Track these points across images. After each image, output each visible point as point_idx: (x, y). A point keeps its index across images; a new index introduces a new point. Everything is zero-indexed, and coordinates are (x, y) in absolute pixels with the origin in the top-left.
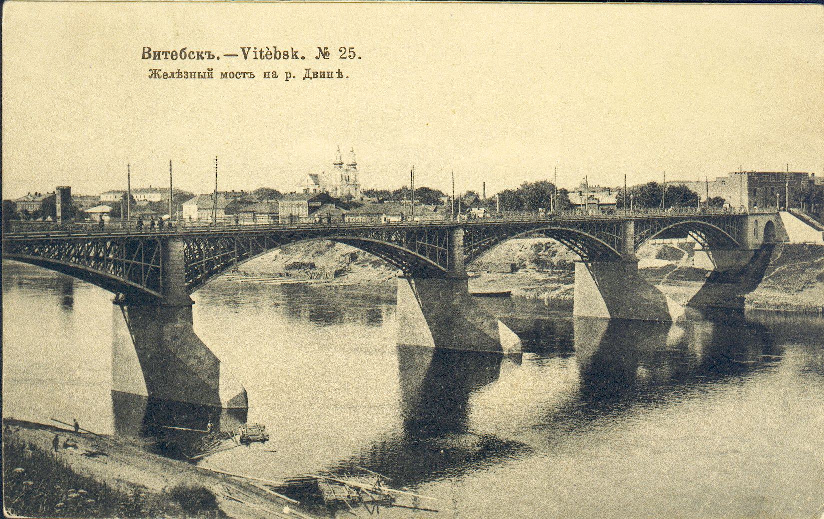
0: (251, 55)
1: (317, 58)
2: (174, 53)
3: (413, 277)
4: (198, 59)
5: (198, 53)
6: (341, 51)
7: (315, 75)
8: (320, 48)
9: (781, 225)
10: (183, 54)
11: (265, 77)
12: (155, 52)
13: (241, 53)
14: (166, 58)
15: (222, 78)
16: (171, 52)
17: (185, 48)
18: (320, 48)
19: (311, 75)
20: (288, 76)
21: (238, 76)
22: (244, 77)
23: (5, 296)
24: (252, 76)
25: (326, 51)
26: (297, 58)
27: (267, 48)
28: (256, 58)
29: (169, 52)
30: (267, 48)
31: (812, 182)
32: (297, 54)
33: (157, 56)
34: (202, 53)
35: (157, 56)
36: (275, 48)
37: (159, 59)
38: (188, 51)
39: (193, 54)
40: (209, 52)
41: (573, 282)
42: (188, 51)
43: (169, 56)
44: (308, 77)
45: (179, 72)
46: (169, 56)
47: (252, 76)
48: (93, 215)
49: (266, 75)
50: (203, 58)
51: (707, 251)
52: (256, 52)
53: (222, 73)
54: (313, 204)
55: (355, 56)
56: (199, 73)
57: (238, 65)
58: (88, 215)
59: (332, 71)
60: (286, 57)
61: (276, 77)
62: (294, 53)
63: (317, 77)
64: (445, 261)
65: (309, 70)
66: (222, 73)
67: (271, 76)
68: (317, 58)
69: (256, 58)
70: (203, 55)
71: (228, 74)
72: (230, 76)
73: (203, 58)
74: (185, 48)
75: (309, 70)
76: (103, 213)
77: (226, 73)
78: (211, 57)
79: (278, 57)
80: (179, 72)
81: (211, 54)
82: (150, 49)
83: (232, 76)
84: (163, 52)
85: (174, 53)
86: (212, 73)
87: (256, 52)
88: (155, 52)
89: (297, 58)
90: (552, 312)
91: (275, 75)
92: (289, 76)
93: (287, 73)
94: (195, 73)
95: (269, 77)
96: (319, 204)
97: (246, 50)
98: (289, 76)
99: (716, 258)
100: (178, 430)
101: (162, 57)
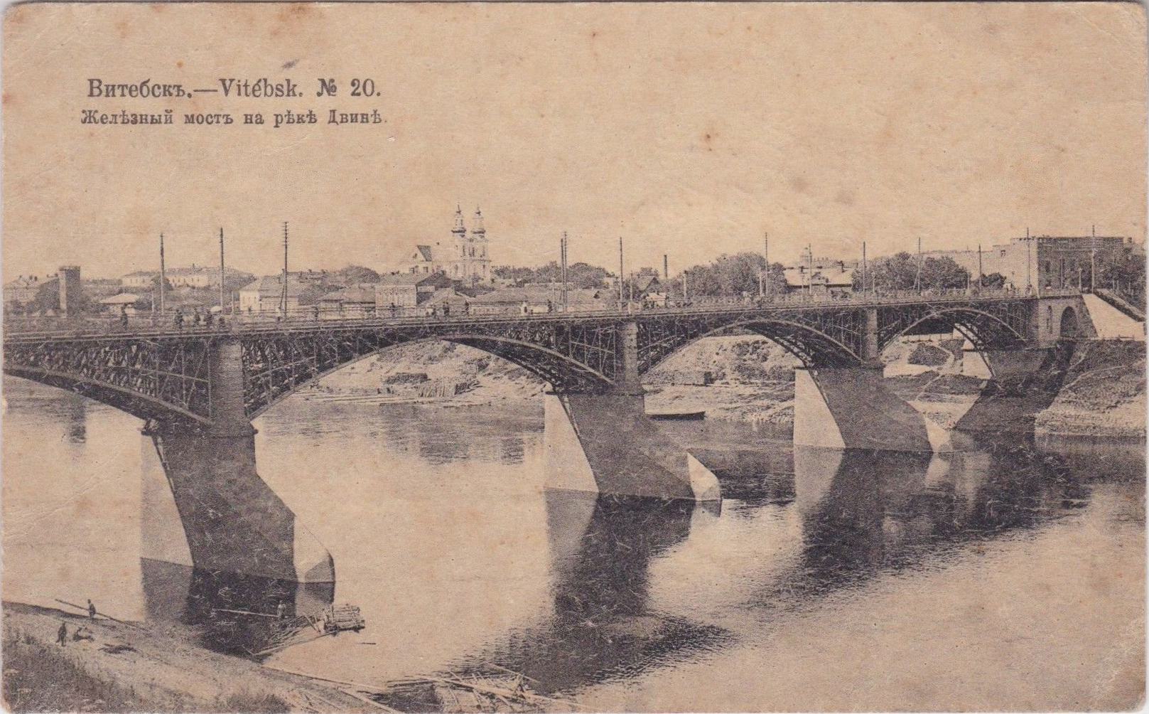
1: (319, 94)
2: (134, 88)
4: (165, 95)
12: (107, 86)
14: (123, 95)
15: (186, 123)
16: (129, 86)
19: (338, 119)
21: (210, 120)
25: (331, 85)
34: (170, 86)
35: (110, 91)
37: (114, 96)
38: (150, 85)
40: (179, 87)
45: (124, 115)
46: (126, 92)
50: (171, 94)
60: (280, 93)
62: (291, 87)
63: (347, 121)
66: (187, 116)
70: (171, 90)
71: (195, 118)
73: (171, 94)
77: (192, 116)
78: (181, 93)
80: (124, 115)
84: (119, 86)
85: (134, 88)
88: (107, 86)
97: (228, 83)
101: (118, 92)
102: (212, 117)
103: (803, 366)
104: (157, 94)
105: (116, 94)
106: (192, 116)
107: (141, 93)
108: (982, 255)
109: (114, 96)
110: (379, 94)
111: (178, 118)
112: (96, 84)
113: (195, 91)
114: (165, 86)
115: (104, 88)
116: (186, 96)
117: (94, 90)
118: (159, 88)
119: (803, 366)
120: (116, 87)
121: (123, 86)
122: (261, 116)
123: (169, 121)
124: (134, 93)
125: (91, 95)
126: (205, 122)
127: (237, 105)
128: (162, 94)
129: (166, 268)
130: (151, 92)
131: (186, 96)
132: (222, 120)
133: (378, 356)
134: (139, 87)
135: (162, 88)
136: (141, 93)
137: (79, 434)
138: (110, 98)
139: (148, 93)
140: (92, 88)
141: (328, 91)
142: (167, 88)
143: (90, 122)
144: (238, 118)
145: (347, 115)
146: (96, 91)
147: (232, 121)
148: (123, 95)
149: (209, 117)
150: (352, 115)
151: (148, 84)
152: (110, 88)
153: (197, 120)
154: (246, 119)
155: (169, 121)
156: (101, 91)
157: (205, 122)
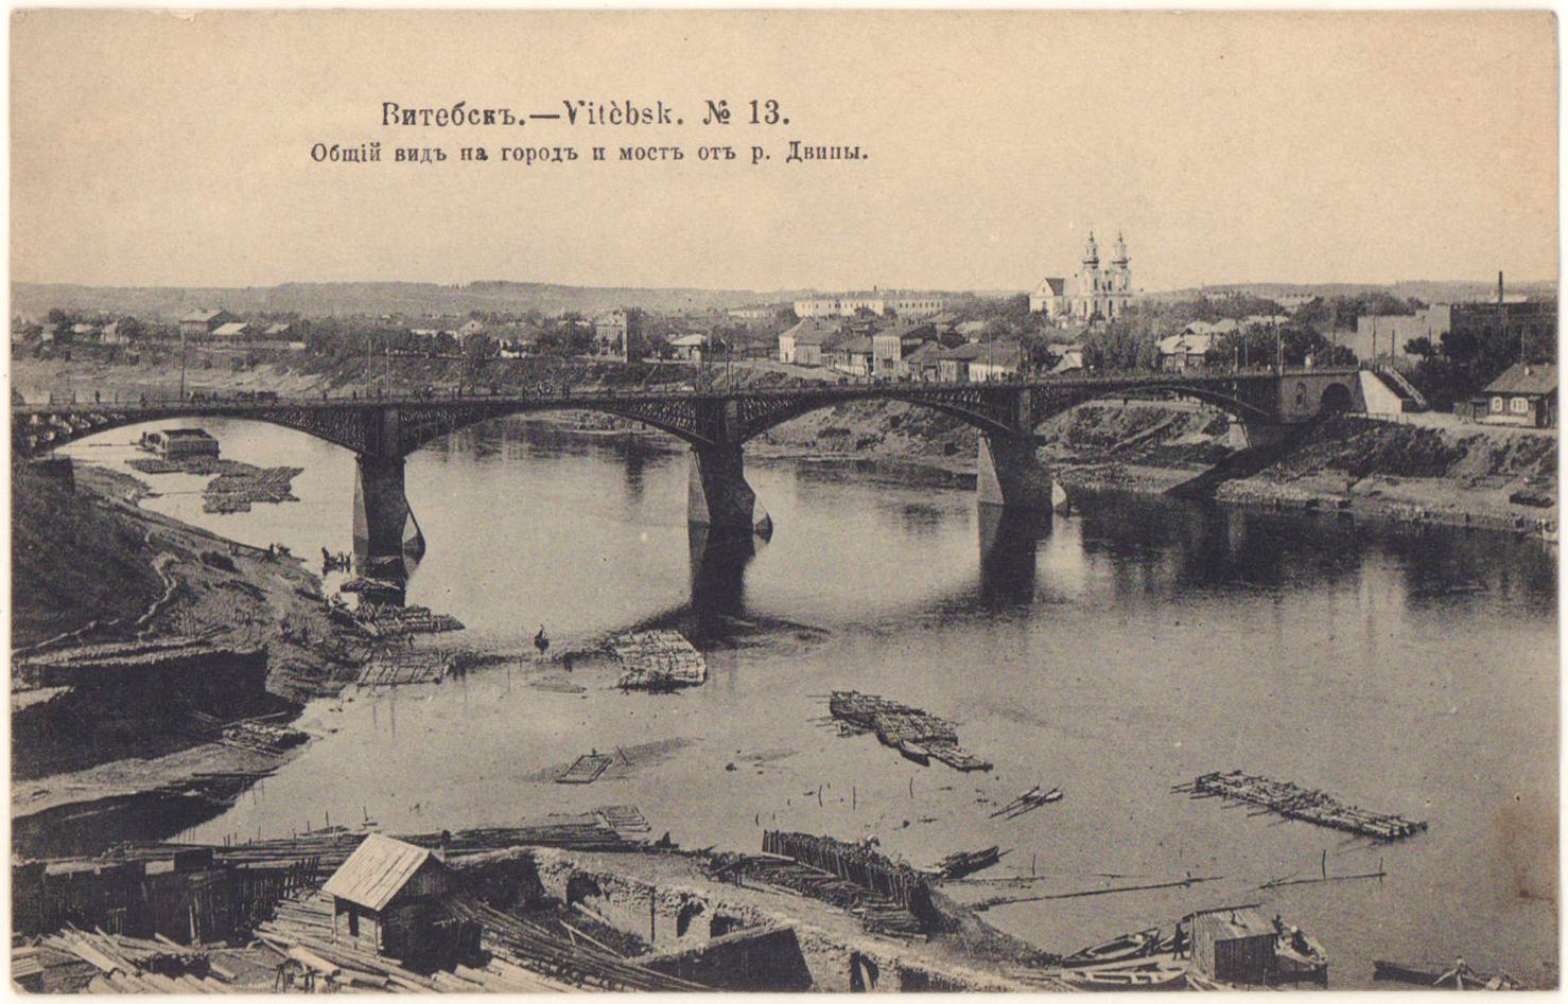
0: (582, 115)
1: (706, 122)
2: (442, 114)
3: (1247, 423)
5: (486, 112)
6: (768, 106)
7: (809, 152)
8: (711, 105)
9: (1359, 388)
12: (405, 112)
13: (564, 113)
17: (462, 104)
18: (711, 105)
19: (801, 153)
20: (757, 153)
24: (483, 156)
25: (723, 108)
27: (613, 103)
28: (592, 122)
30: (613, 103)
32: (668, 114)
33: (409, 117)
35: (409, 117)
36: (628, 103)
37: (414, 123)
41: (976, 456)
42: (466, 110)
43: (432, 119)
44: (796, 157)
46: (432, 119)
48: (680, 350)
49: (466, 153)
51: (1241, 424)
53: (622, 150)
54: (908, 342)
55: (438, 117)
56: (847, 149)
57: (559, 134)
58: (674, 349)
60: (648, 120)
61: (485, 158)
62: (663, 112)
65: (796, 144)
66: (622, 150)
68: (706, 122)
69: (592, 122)
71: (633, 152)
74: (462, 104)
75: (796, 144)
76: (692, 346)
77: (630, 150)
78: (510, 120)
79: (632, 119)
82: (397, 108)
83: (544, 152)
85: (442, 114)
87: (591, 111)
88: (405, 112)
91: (483, 156)
92: (758, 155)
93: (754, 149)
94: (470, 150)
96: (919, 341)
98: (758, 155)
99: (1252, 433)
100: (59, 634)
101: (420, 119)
103: (361, 920)
105: (417, 121)
106: (630, 150)
108: (1378, 878)
110: (786, 121)
111: (388, 153)
112: (391, 108)
113: (532, 117)
115: (400, 114)
119: (361, 920)
120: (417, 114)
121: (426, 112)
123: (376, 157)
126: (646, 157)
127: (582, 136)
128: (483, 120)
129: (1505, 286)
130: (328, 150)
133: (1068, 443)
138: (410, 126)
141: (718, 116)
144: (454, 154)
146: (390, 118)
147: (734, 155)
148: (426, 124)
150: (410, 151)
151: (462, 108)
154: (397, 155)
155: (376, 157)
157: (646, 157)
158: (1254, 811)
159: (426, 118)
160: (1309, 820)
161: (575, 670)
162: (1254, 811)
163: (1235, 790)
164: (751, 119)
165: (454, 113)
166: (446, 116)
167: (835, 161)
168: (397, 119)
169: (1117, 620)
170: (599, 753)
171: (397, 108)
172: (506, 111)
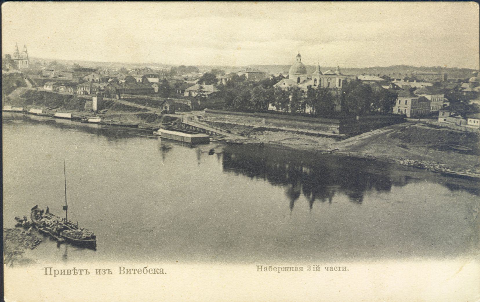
2: (140, 270)
10: (145, 271)
11: (97, 274)
22: (81, 274)
23: (8, 272)
26: (164, 274)
28: (314, 270)
29: (136, 269)
31: (346, 193)
37: (130, 273)
39: (152, 270)
40: (109, 270)
43: (136, 272)
46: (136, 272)
47: (87, 273)
52: (314, 268)
59: (120, 275)
64: (415, 118)
67: (329, 269)
70: (159, 271)
72: (335, 269)
78: (88, 273)
81: (110, 271)
84: (79, 270)
85: (140, 270)
86: (319, 268)
87: (314, 268)
89: (164, 274)
90: (469, 165)
95: (64, 274)
101: (132, 272)
102: (337, 268)
104: (336, 270)
107: (143, 272)
109: (130, 273)
112: (122, 269)
114: (155, 269)
115: (125, 271)
116: (159, 269)
117: (121, 271)
118: (152, 270)
120: (131, 270)
121: (81, 270)
122: (163, 270)
124: (140, 273)
125: (120, 273)
130: (148, 272)
131: (159, 269)
132: (107, 272)
134: (142, 270)
135: (153, 270)
136: (143, 272)
137: (16, 219)
139: (147, 272)
140: (120, 270)
142: (156, 270)
143: (286, 271)
145: (295, 270)
146: (122, 272)
148: (134, 273)
149: (151, 270)
152: (63, 271)
153: (335, 269)
154: (97, 272)
156: (124, 272)
158: (341, 82)
159: (340, 269)
160: (193, 122)
161: (366, 199)
162: (341, 82)
163: (318, 81)
164: (119, 273)
165: (144, 270)
166: (141, 271)
167: (63, 275)
168: (124, 272)
169: (11, 106)
170: (56, 244)
171: (124, 268)
172: (86, 270)
